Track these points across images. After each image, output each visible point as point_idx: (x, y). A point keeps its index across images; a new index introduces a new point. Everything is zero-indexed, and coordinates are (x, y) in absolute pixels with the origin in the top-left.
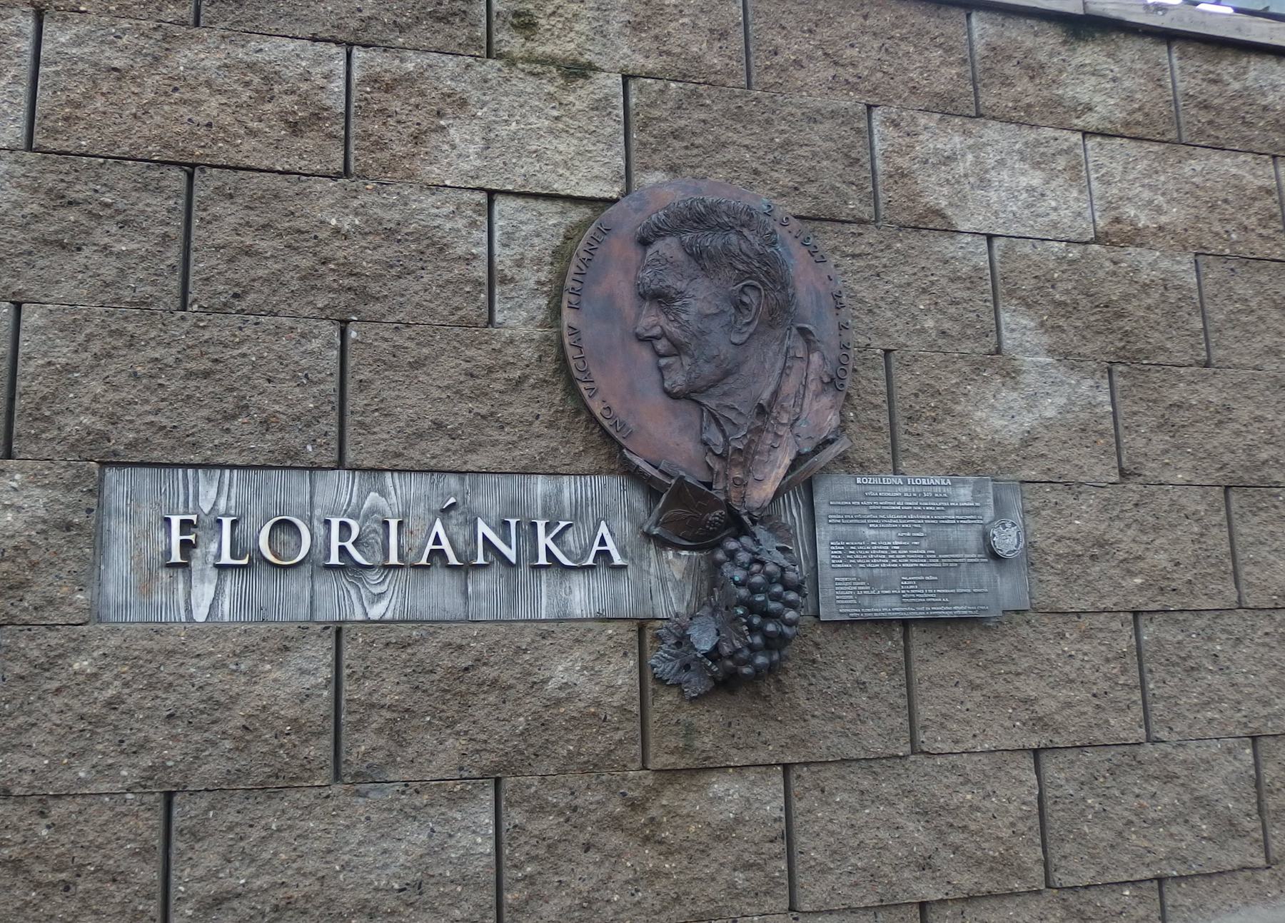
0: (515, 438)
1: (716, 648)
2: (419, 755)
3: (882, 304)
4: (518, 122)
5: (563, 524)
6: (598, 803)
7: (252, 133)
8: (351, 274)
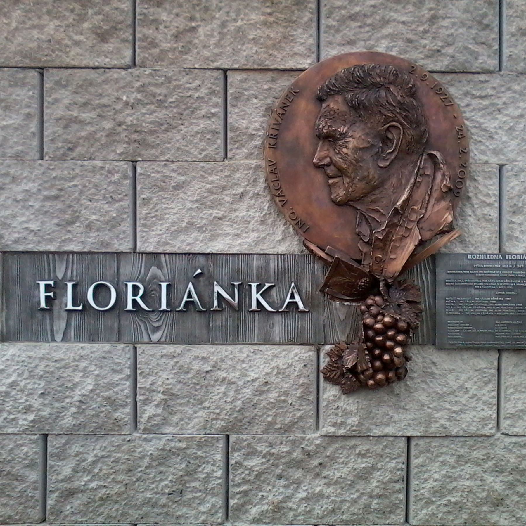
0: (239, 232)
1: (355, 366)
2: (182, 420)
3: (500, 131)
4: (242, 19)
5: (267, 285)
6: (286, 452)
7: (77, 43)
8: (136, 131)
